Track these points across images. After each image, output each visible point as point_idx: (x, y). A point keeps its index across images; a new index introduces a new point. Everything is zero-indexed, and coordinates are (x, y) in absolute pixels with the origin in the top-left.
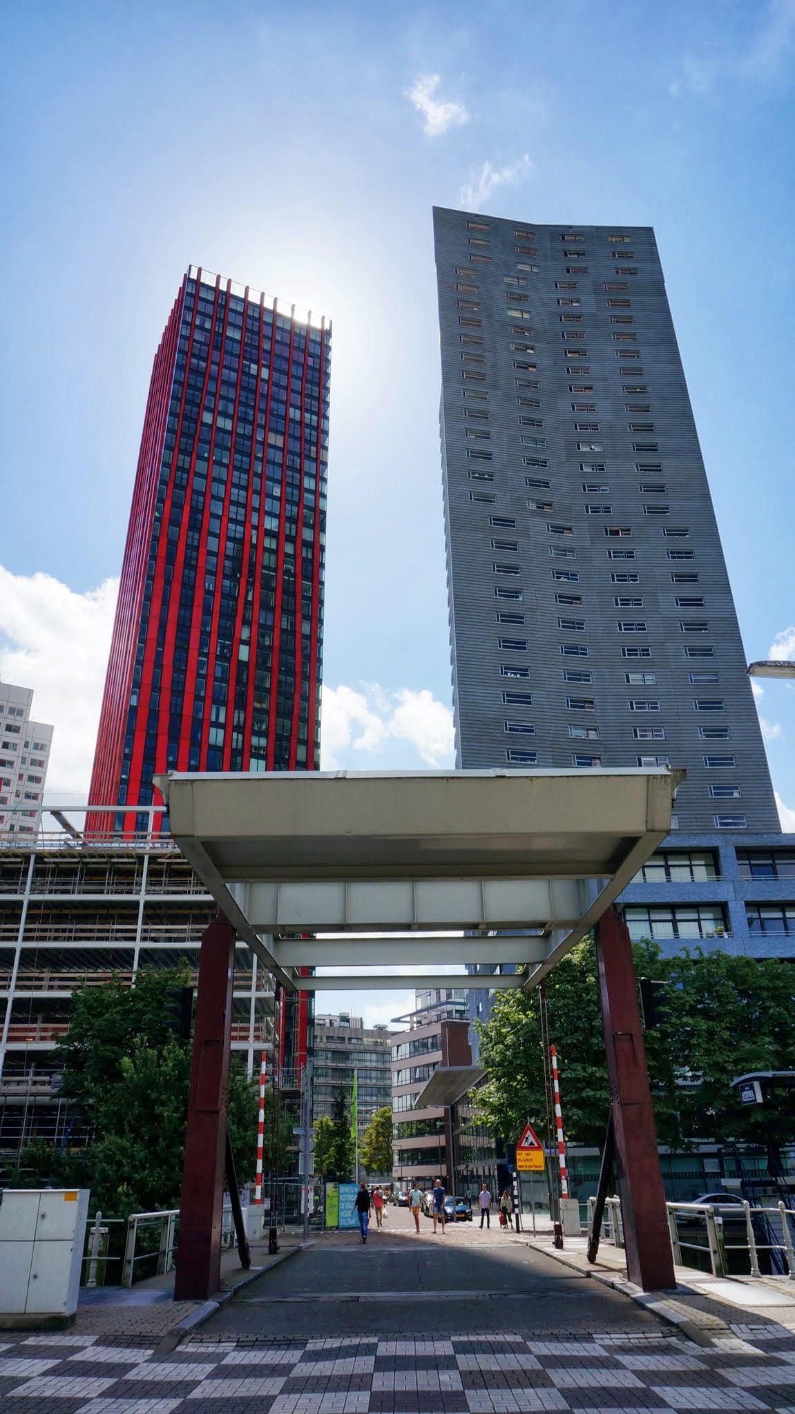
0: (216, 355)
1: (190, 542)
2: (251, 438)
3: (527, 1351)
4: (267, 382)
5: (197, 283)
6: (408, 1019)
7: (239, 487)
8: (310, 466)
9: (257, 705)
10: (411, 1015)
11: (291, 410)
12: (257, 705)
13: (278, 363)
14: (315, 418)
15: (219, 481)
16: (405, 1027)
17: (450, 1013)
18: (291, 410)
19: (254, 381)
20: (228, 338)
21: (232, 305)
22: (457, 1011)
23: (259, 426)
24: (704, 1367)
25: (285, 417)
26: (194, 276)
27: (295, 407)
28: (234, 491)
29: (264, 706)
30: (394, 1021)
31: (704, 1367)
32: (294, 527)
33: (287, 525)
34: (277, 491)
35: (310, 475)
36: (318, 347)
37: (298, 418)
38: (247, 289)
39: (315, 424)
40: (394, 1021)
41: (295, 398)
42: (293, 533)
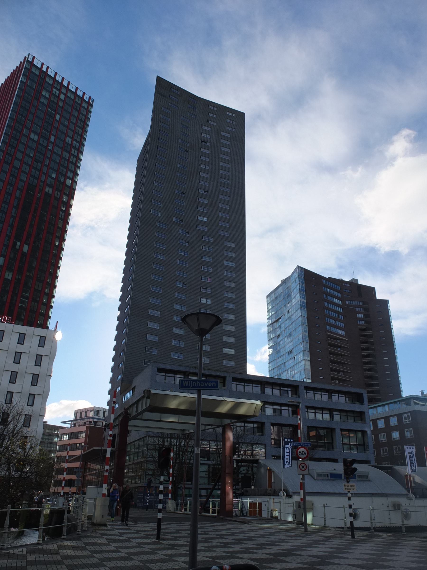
0: (35, 103)
1: (7, 191)
2: (46, 147)
3: (99, 559)
4: (58, 121)
5: (31, 63)
6: (70, 422)
7: (36, 169)
8: (70, 174)
9: (28, 274)
10: (71, 421)
11: (68, 138)
12: (28, 274)
13: (64, 114)
14: (78, 144)
15: (27, 164)
16: (67, 426)
17: (90, 422)
18: (68, 138)
19: (44, 149)
20: (46, 82)
21: (47, 79)
22: (94, 422)
23: (45, 165)
24: (127, 555)
25: (64, 141)
26: (30, 59)
27: (70, 137)
28: (33, 170)
29: (31, 275)
30: (62, 422)
31: (127, 555)
32: (59, 193)
33: (56, 192)
34: (54, 176)
35: (71, 171)
36: (85, 111)
37: (70, 142)
38: (56, 73)
39: (77, 147)
40: (62, 422)
41: (71, 133)
42: (58, 197)
